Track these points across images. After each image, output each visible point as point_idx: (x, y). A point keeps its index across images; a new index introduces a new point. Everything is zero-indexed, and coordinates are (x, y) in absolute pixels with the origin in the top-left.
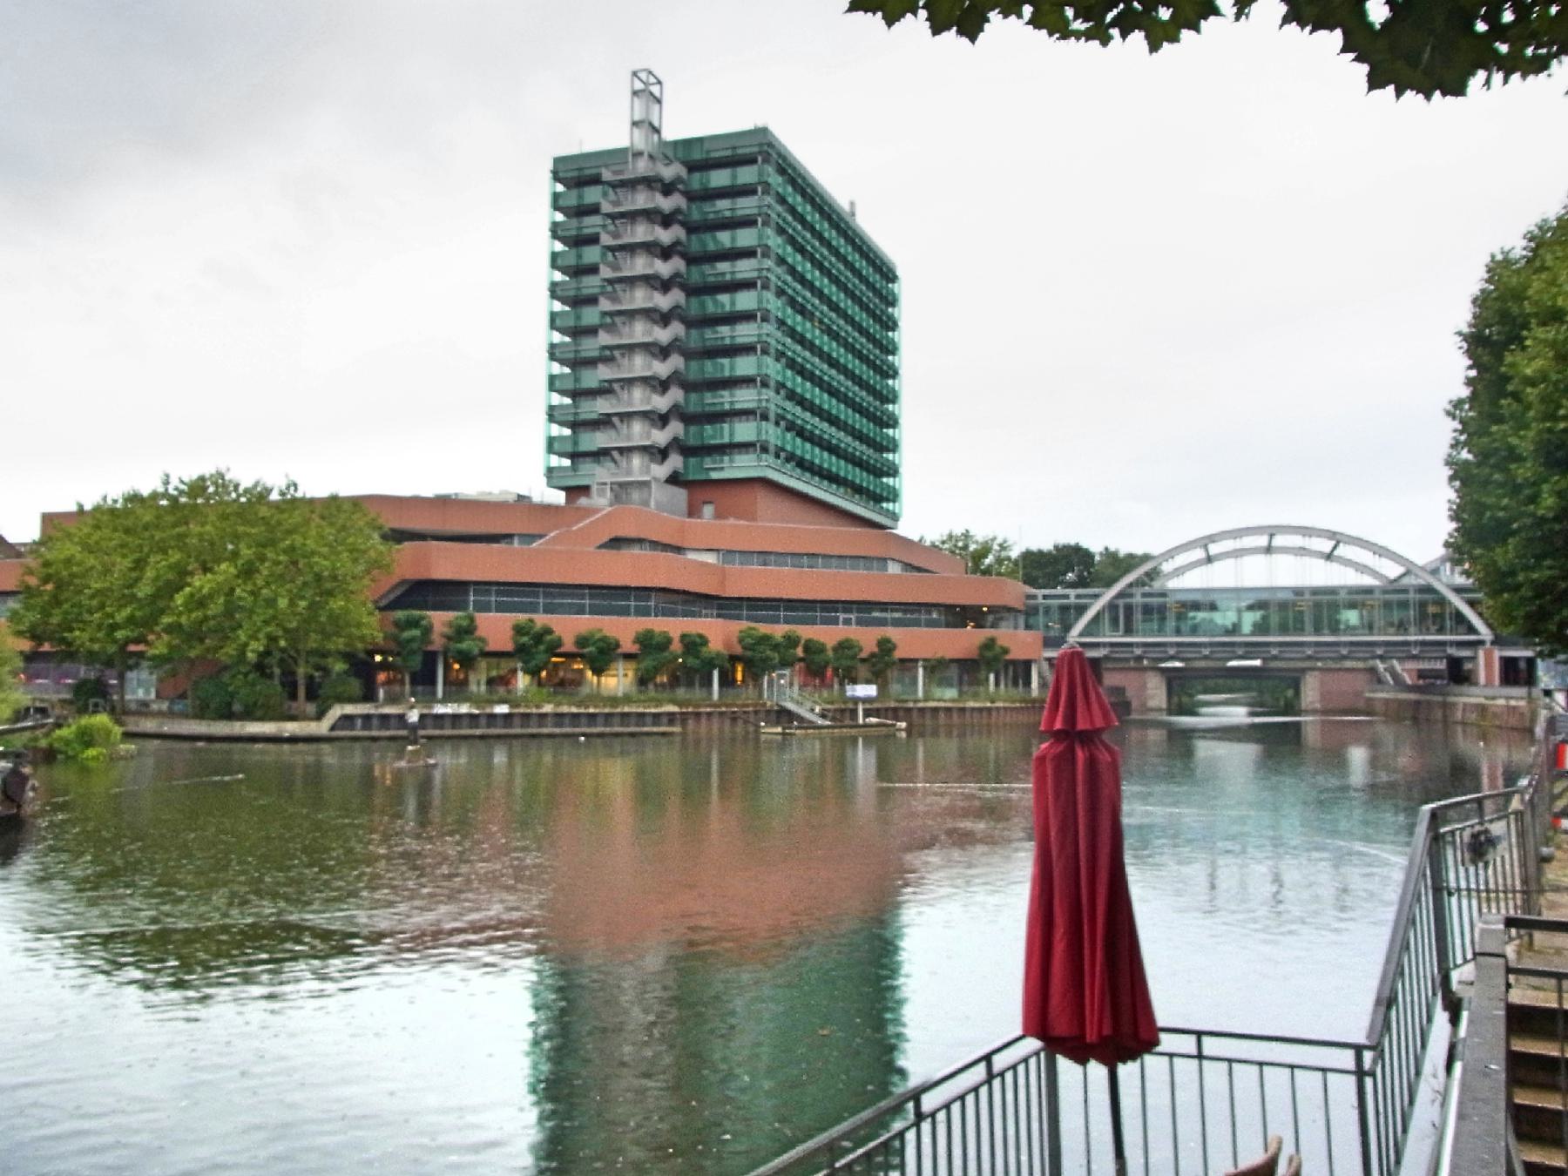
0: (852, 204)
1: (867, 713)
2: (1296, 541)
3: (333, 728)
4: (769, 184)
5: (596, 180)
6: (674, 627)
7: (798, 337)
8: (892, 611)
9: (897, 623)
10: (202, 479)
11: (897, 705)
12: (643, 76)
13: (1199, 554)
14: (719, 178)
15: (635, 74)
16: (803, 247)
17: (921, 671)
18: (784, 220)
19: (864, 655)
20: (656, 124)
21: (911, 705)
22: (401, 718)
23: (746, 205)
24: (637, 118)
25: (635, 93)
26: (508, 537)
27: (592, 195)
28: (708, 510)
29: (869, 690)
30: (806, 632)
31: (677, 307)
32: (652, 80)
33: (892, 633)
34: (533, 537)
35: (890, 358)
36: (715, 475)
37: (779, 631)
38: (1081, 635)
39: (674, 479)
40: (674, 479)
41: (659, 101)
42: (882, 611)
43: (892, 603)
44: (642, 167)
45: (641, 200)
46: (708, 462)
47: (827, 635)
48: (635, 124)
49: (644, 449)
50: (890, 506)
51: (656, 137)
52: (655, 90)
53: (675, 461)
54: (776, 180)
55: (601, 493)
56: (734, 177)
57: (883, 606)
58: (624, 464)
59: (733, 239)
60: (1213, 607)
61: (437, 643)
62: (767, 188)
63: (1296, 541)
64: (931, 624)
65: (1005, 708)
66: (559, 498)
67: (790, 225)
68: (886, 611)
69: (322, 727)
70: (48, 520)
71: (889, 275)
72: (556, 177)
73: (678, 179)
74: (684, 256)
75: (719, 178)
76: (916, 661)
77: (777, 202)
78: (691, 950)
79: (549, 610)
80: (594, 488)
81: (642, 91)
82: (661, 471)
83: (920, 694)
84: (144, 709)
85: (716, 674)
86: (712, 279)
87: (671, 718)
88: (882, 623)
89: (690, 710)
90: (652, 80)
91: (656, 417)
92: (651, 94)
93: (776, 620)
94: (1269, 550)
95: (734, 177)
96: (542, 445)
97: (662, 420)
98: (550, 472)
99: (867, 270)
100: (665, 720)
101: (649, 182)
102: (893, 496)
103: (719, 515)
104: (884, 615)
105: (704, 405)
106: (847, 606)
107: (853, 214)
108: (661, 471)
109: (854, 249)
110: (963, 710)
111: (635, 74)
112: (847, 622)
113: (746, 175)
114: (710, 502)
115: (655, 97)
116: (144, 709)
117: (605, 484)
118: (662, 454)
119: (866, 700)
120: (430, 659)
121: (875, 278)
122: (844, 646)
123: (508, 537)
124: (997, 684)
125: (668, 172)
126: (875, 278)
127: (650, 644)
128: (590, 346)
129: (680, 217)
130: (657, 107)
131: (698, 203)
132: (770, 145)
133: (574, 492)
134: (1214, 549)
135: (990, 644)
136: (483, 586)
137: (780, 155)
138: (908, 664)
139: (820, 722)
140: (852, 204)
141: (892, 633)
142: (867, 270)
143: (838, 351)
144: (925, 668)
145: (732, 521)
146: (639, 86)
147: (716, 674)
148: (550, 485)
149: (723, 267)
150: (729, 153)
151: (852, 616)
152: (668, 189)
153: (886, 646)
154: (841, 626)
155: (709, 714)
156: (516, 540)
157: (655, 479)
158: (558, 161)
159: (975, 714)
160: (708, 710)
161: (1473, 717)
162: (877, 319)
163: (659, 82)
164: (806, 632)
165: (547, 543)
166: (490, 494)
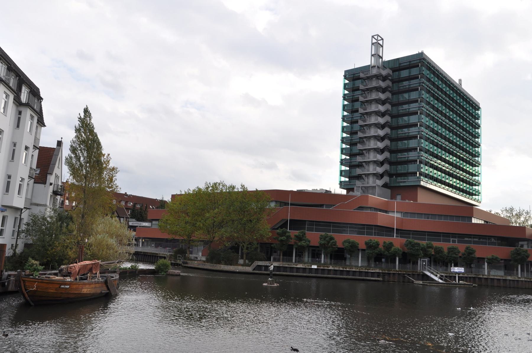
0: (460, 80)
1: (460, 279)
3: (254, 270)
4: (423, 74)
5: (359, 78)
6: (381, 240)
7: (436, 132)
8: (474, 238)
9: (475, 243)
10: (71, 146)
11: (475, 276)
12: (376, 37)
14: (404, 74)
15: (373, 37)
16: (438, 97)
17: (486, 264)
18: (429, 88)
19: (460, 255)
20: (381, 55)
21: (481, 277)
22: (267, 267)
23: (414, 83)
24: (373, 53)
25: (373, 44)
26: (322, 206)
27: (358, 83)
28: (399, 197)
29: (462, 270)
30: (435, 244)
31: (387, 122)
32: (379, 38)
33: (472, 246)
34: (331, 206)
35: (477, 139)
36: (402, 184)
37: (424, 243)
39: (385, 186)
40: (385, 186)
41: (382, 46)
44: (375, 72)
45: (374, 83)
46: (399, 179)
47: (444, 246)
48: (372, 55)
49: (374, 174)
50: (477, 197)
51: (381, 60)
52: (381, 42)
53: (386, 179)
54: (426, 72)
55: (358, 191)
56: (410, 73)
57: (469, 236)
58: (366, 180)
59: (409, 96)
61: (292, 242)
62: (423, 76)
64: (490, 244)
65: (525, 281)
66: (344, 192)
67: (448, 102)
68: (471, 238)
69: (249, 269)
70: (173, 196)
71: (476, 107)
72: (345, 77)
73: (389, 75)
74: (390, 103)
75: (404, 74)
77: (427, 81)
79: (334, 231)
80: (355, 188)
81: (376, 43)
82: (380, 182)
83: (486, 274)
84: (196, 259)
85: (397, 259)
86: (401, 111)
87: (378, 275)
88: (469, 242)
89: (386, 272)
90: (379, 38)
91: (379, 163)
92: (379, 44)
93: (424, 239)
95: (410, 73)
96: (338, 173)
97: (381, 164)
100: (376, 275)
101: (378, 77)
102: (478, 193)
103: (402, 199)
104: (470, 239)
105: (397, 158)
106: (454, 235)
107: (461, 84)
108: (380, 182)
109: (463, 100)
110: (505, 280)
111: (373, 37)
112: (454, 241)
113: (414, 71)
114: (400, 194)
115: (381, 45)
116: (196, 259)
117: (359, 187)
118: (381, 176)
119: (459, 273)
120: (291, 247)
121: (469, 108)
122: (451, 250)
123: (322, 206)
124: (522, 270)
125: (384, 73)
126: (469, 108)
127: (370, 246)
128: (356, 138)
129: (389, 89)
130: (381, 49)
131: (396, 83)
132: (424, 59)
133: (349, 190)
135: (518, 253)
136: (312, 223)
137: (428, 63)
138: (481, 260)
139: (440, 281)
140: (460, 80)
141: (472, 246)
142: (467, 106)
144: (488, 263)
146: (374, 41)
147: (397, 259)
148: (341, 187)
149: (406, 107)
150: (408, 64)
151: (456, 239)
152: (384, 79)
153: (470, 252)
155: (394, 274)
157: (378, 186)
158: (346, 72)
160: (393, 272)
161: (502, 284)
162: (472, 125)
163: (382, 39)
164: (435, 244)
165: (335, 208)
166: (317, 190)
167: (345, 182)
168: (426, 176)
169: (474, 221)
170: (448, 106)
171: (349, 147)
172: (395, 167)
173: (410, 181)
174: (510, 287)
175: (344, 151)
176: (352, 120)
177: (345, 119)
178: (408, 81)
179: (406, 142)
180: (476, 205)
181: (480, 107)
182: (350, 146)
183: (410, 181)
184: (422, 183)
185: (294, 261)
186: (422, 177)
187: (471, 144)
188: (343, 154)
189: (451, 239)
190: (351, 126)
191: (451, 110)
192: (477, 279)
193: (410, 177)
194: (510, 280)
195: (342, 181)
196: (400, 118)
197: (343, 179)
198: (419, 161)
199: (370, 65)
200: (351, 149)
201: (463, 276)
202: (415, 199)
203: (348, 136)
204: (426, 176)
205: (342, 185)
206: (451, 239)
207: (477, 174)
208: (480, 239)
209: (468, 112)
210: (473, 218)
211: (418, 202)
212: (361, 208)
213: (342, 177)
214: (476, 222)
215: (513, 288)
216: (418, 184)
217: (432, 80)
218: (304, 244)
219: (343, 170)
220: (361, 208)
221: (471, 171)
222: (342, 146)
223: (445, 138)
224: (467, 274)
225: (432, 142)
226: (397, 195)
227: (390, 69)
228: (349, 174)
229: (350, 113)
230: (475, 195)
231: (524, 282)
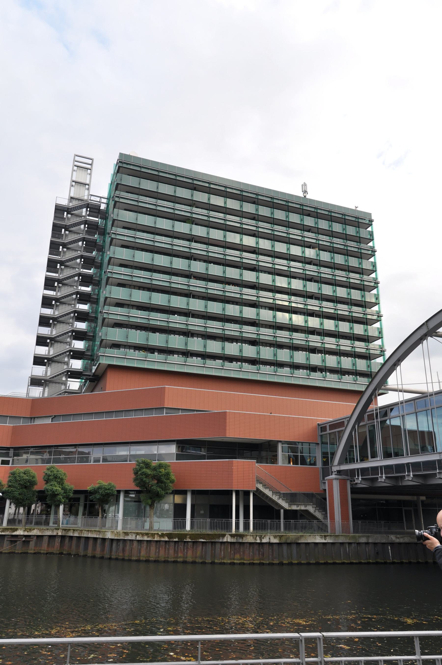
38: (340, 463)
159: (237, 546)
174: (110, 559)
181: (373, 218)
192: (67, 540)
194: (112, 540)
201: (26, 533)
215: (136, 561)
224: (40, 530)
231: (135, 544)
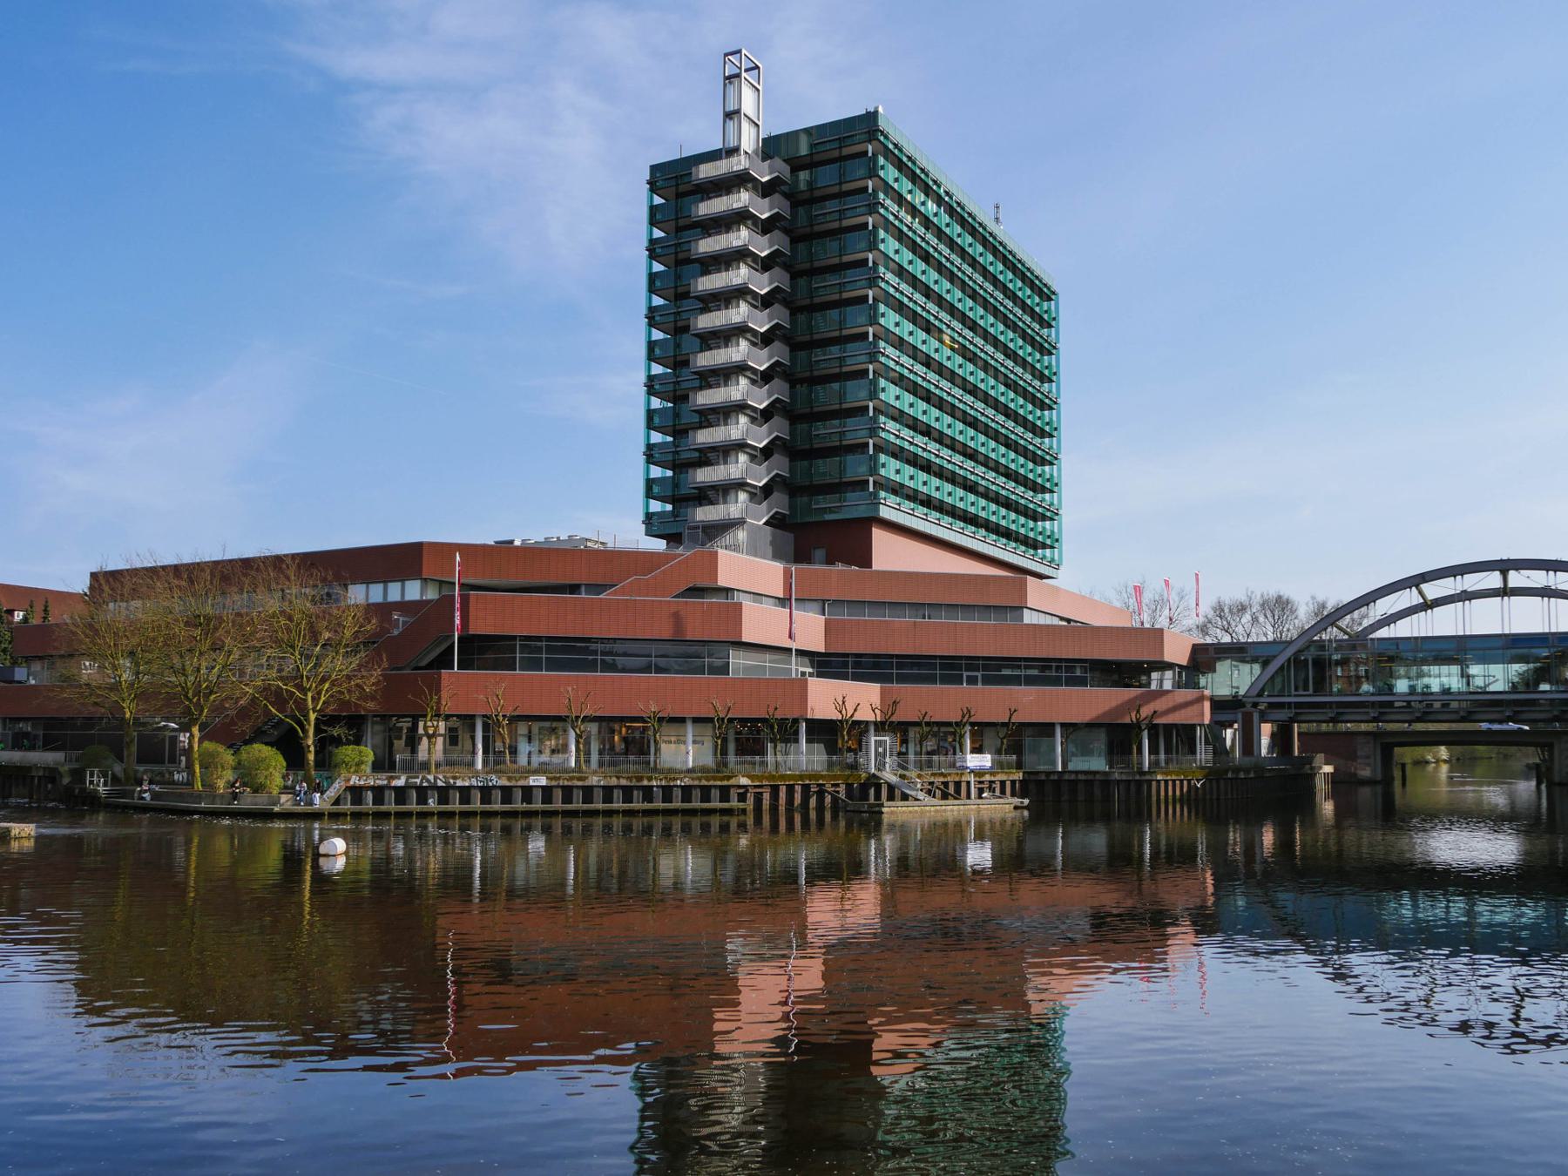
2: (1538, 578)
8: (1027, 667)
13: (1493, 580)
26: (574, 589)
42: (1013, 667)
43: (1026, 659)
46: (822, 502)
60: (1099, 920)
63: (1538, 578)
66: (660, 545)
68: (1019, 667)
72: (654, 187)
76: (1052, 725)
78: (1371, 678)
94: (1505, 592)
98: (649, 518)
99: (1025, 293)
123: (574, 589)
124: (1154, 750)
133: (673, 539)
134: (1516, 579)
142: (1025, 293)
143: (977, 377)
145: (840, 567)
148: (649, 533)
151: (979, 674)
154: (980, 686)
156: (583, 589)
167: (661, 514)
168: (897, 489)
169: (1029, 618)
170: (992, 308)
171: (671, 439)
172: (805, 463)
173: (853, 507)
175: (657, 420)
176: (675, 391)
177: (657, 318)
178: (837, 201)
179: (836, 386)
180: (1047, 573)
182: (675, 404)
183: (853, 507)
184: (885, 513)
185: (479, 765)
186: (883, 494)
187: (1029, 396)
188: (655, 429)
189: (965, 674)
190: (675, 339)
191: (970, 292)
193: (848, 495)
194: (1118, 781)
195: (653, 514)
196: (818, 315)
197: (656, 506)
198: (874, 445)
199: (720, 150)
200: (675, 483)
202: (866, 561)
203: (669, 371)
204: (897, 489)
205: (652, 524)
206: (965, 674)
207: (1048, 485)
208: (1043, 669)
209: (1028, 310)
210: (1025, 610)
211: (875, 566)
212: (696, 591)
213: (652, 502)
214: (1035, 621)
216: (1459, 748)
217: (935, 221)
218: (1230, 851)
219: (655, 410)
220: (696, 591)
221: (1031, 476)
222: (649, 403)
223: (952, 445)
225: (914, 389)
226: (815, 549)
227: (784, 161)
228: (674, 491)
229: (673, 299)
230: (1044, 546)
